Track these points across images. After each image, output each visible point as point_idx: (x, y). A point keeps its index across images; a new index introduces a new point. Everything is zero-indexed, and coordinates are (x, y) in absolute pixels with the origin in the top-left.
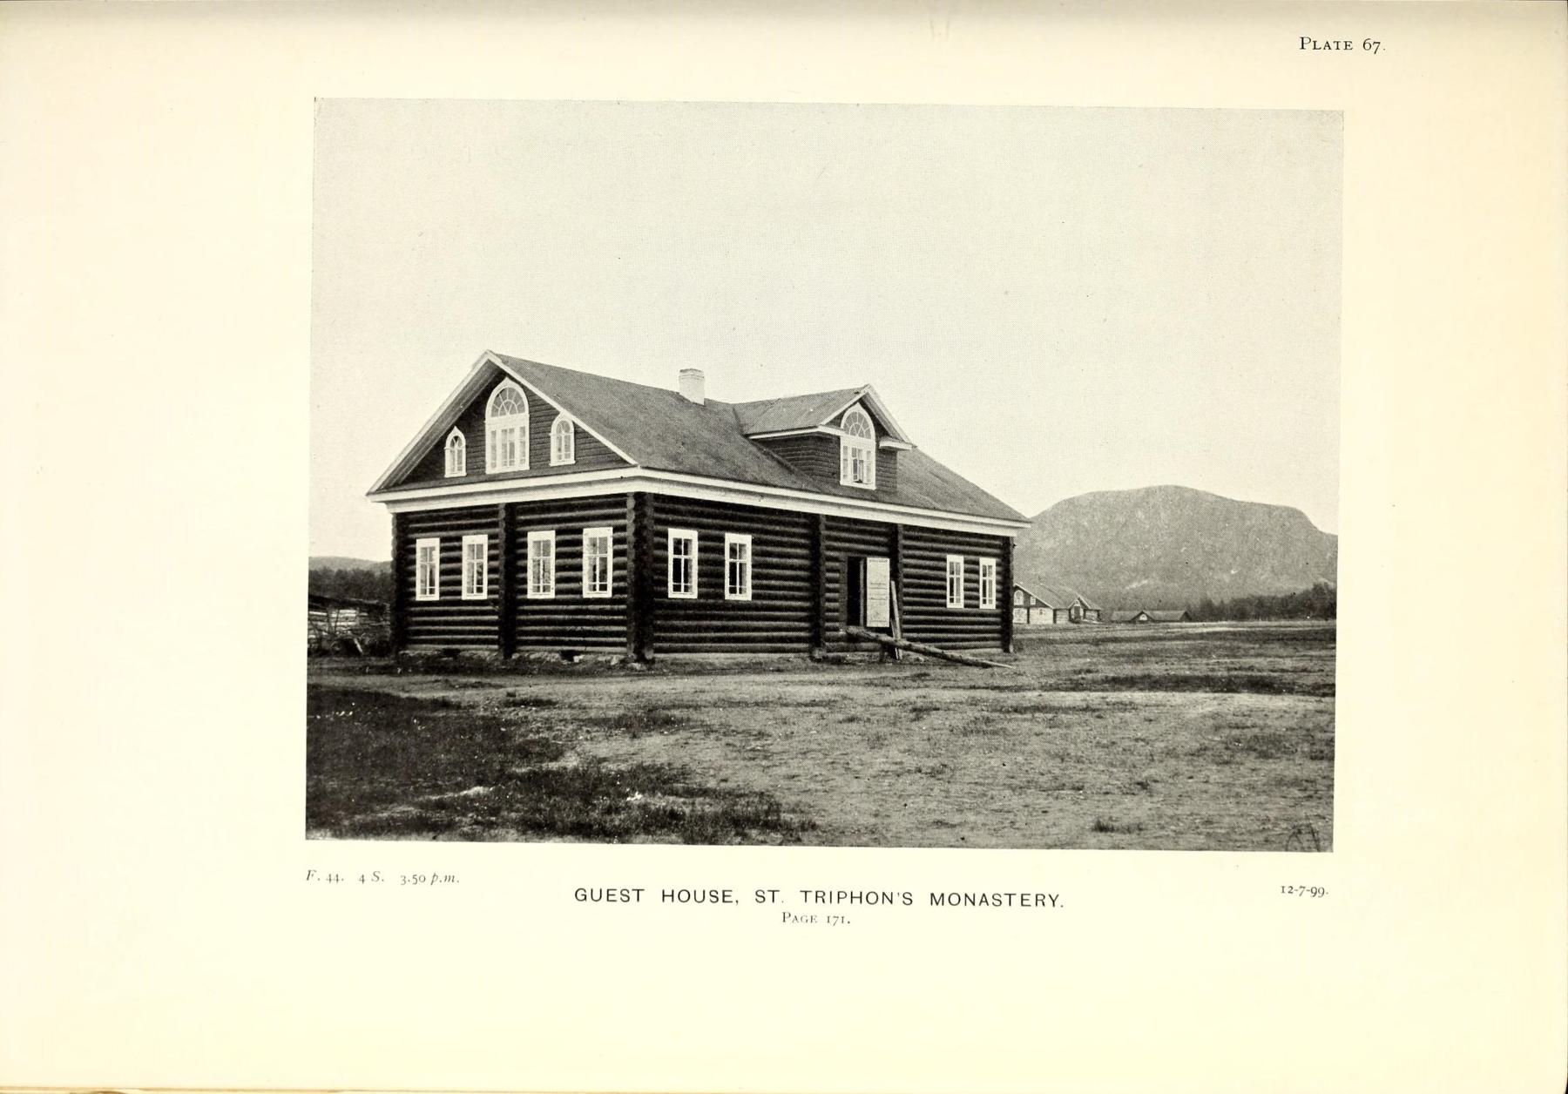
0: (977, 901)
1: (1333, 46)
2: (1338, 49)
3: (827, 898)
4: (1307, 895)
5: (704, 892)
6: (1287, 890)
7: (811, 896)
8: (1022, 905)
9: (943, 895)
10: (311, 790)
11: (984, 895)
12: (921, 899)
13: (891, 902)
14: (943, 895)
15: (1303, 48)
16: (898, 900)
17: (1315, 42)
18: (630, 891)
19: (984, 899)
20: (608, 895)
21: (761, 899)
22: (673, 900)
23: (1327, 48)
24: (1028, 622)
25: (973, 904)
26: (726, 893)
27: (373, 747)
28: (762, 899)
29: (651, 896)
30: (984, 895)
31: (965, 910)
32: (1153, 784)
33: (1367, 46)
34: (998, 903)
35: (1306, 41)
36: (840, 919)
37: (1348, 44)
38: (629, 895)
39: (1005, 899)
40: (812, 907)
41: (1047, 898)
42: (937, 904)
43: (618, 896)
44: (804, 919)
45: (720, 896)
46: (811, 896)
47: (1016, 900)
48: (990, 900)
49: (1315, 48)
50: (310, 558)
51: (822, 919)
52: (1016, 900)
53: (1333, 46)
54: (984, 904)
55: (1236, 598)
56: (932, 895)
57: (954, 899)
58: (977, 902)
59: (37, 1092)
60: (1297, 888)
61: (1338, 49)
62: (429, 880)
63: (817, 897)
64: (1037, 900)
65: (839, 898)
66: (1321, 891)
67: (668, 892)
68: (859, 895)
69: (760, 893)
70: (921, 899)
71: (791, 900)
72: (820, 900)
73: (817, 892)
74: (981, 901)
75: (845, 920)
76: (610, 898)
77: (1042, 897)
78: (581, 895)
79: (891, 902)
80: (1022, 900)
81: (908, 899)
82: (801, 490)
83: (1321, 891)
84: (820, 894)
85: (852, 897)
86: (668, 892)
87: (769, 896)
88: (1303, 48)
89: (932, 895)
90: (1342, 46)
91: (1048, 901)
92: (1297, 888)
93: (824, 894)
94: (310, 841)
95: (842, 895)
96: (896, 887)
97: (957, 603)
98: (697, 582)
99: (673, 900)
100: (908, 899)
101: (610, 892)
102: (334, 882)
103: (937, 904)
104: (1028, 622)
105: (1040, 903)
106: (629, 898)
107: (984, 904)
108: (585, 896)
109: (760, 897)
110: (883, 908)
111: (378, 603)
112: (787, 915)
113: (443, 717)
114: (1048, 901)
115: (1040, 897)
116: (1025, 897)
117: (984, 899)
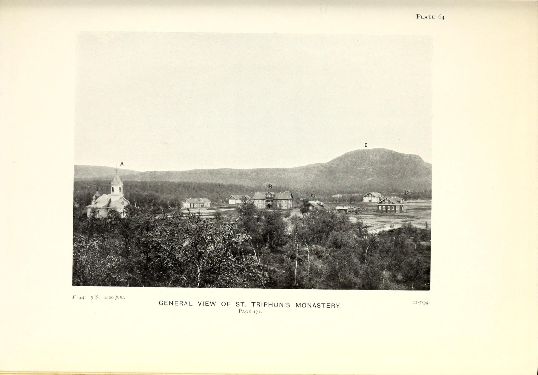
0: (312, 306)
2: (430, 18)
3: (261, 305)
5: (162, 303)
6: (415, 302)
7: (255, 304)
8: (327, 307)
9: (300, 304)
11: (314, 304)
12: (293, 305)
13: (283, 306)
14: (300, 304)
15: (418, 18)
16: (285, 306)
19: (314, 305)
20: (206, 304)
21: (238, 305)
25: (311, 307)
27: (239, 257)
29: (218, 304)
30: (314, 304)
31: (308, 309)
34: (319, 307)
35: (419, 16)
36: (258, 312)
37: (433, 16)
38: (320, 305)
39: (322, 305)
40: (256, 308)
41: (336, 305)
42: (298, 307)
43: (209, 304)
44: (247, 312)
46: (255, 304)
47: (325, 305)
48: (316, 306)
50: (76, 167)
52: (325, 305)
54: (314, 307)
55: (416, 227)
56: (297, 304)
57: (276, 305)
58: (312, 306)
59: (179, 374)
60: (419, 302)
61: (430, 18)
62: (115, 298)
63: (257, 304)
64: (180, 303)
65: (265, 305)
66: (427, 303)
67: (270, 303)
68: (228, 305)
69: (238, 303)
71: (248, 306)
72: (258, 305)
73: (180, 302)
74: (313, 306)
75: (260, 312)
76: (207, 305)
77: (182, 302)
79: (283, 306)
80: (327, 305)
81: (288, 305)
83: (427, 303)
84: (258, 303)
85: (269, 305)
86: (270, 303)
88: (418, 18)
89: (297, 304)
90: (431, 17)
91: (336, 306)
92: (419, 302)
93: (335, 305)
94: (74, 286)
95: (266, 304)
96: (285, 302)
98: (205, 199)
100: (288, 305)
101: (228, 303)
102: (82, 299)
103: (298, 307)
105: (333, 307)
106: (320, 306)
107: (314, 307)
108: (163, 303)
109: (238, 304)
111: (336, 206)
112: (241, 310)
113: (367, 251)
114: (336, 306)
115: (333, 305)
117: (314, 305)
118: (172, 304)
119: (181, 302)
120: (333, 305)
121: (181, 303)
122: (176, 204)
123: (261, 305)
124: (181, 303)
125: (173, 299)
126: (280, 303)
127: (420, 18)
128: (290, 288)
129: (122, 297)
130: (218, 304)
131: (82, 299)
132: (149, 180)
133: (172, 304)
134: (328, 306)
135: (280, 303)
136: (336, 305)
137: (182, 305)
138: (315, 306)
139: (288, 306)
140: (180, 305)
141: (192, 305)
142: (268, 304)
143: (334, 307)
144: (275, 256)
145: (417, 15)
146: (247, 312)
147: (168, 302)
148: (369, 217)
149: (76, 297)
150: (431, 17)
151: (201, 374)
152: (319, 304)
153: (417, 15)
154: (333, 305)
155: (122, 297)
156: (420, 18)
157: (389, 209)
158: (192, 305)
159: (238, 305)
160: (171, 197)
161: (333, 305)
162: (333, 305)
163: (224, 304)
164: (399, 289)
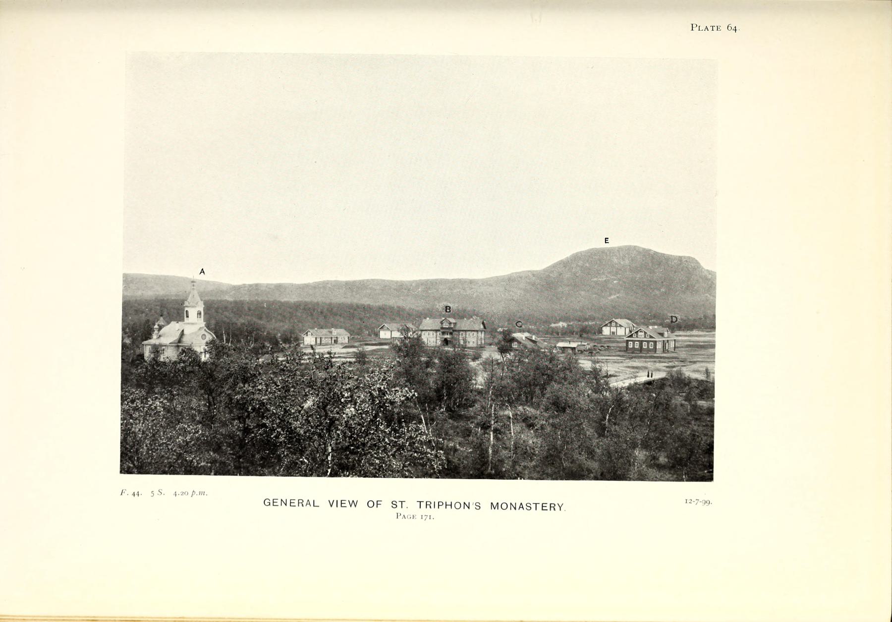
0: (518, 507)
3: (432, 505)
4: (700, 504)
5: (268, 503)
7: (423, 505)
8: (542, 509)
9: (498, 503)
10: (535, 475)
11: (521, 504)
12: (485, 506)
13: (469, 508)
14: (498, 503)
15: (692, 30)
16: (472, 507)
17: (699, 26)
19: (521, 505)
20: (341, 503)
21: (395, 506)
23: (706, 30)
25: (515, 508)
28: (479, 508)
29: (362, 505)
30: (521, 504)
33: (730, 28)
34: (529, 508)
35: (694, 26)
36: (429, 517)
37: (719, 27)
39: (533, 506)
40: (424, 511)
41: (557, 505)
42: (495, 509)
43: (347, 504)
44: (409, 517)
46: (423, 505)
47: (539, 506)
48: (525, 507)
52: (539, 506)
56: (492, 503)
57: (504, 506)
61: (713, 30)
62: (190, 494)
63: (427, 505)
66: (708, 502)
67: (449, 503)
71: (412, 507)
72: (428, 506)
74: (520, 507)
76: (343, 505)
77: (430, 503)
79: (469, 508)
80: (542, 506)
82: (608, 356)
83: (708, 502)
84: (428, 503)
85: (446, 505)
86: (449, 503)
88: (692, 30)
89: (492, 503)
90: (715, 28)
91: (557, 507)
93: (431, 503)
94: (122, 475)
95: (441, 504)
100: (478, 506)
101: (378, 503)
102: (136, 496)
103: (495, 509)
104: (316, 338)
105: (552, 509)
106: (480, 507)
108: (270, 503)
112: (399, 515)
115: (552, 505)
117: (308, 503)
118: (286, 505)
119: (301, 501)
121: (300, 502)
122: (292, 339)
123: (432, 505)
124: (300, 502)
125: (287, 497)
126: (464, 503)
127: (696, 29)
129: (202, 493)
130: (362, 505)
131: (136, 496)
132: (247, 299)
133: (286, 505)
134: (544, 508)
136: (557, 505)
137: (430, 507)
138: (309, 504)
139: (478, 508)
140: (550, 510)
141: (536, 509)
143: (554, 509)
145: (692, 25)
146: (409, 517)
147: (296, 502)
148: (612, 361)
150: (715, 28)
153: (692, 25)
154: (552, 506)
155: (202, 493)
156: (696, 29)
158: (402, 507)
160: (283, 326)
161: (552, 505)
162: (552, 506)
163: (371, 504)
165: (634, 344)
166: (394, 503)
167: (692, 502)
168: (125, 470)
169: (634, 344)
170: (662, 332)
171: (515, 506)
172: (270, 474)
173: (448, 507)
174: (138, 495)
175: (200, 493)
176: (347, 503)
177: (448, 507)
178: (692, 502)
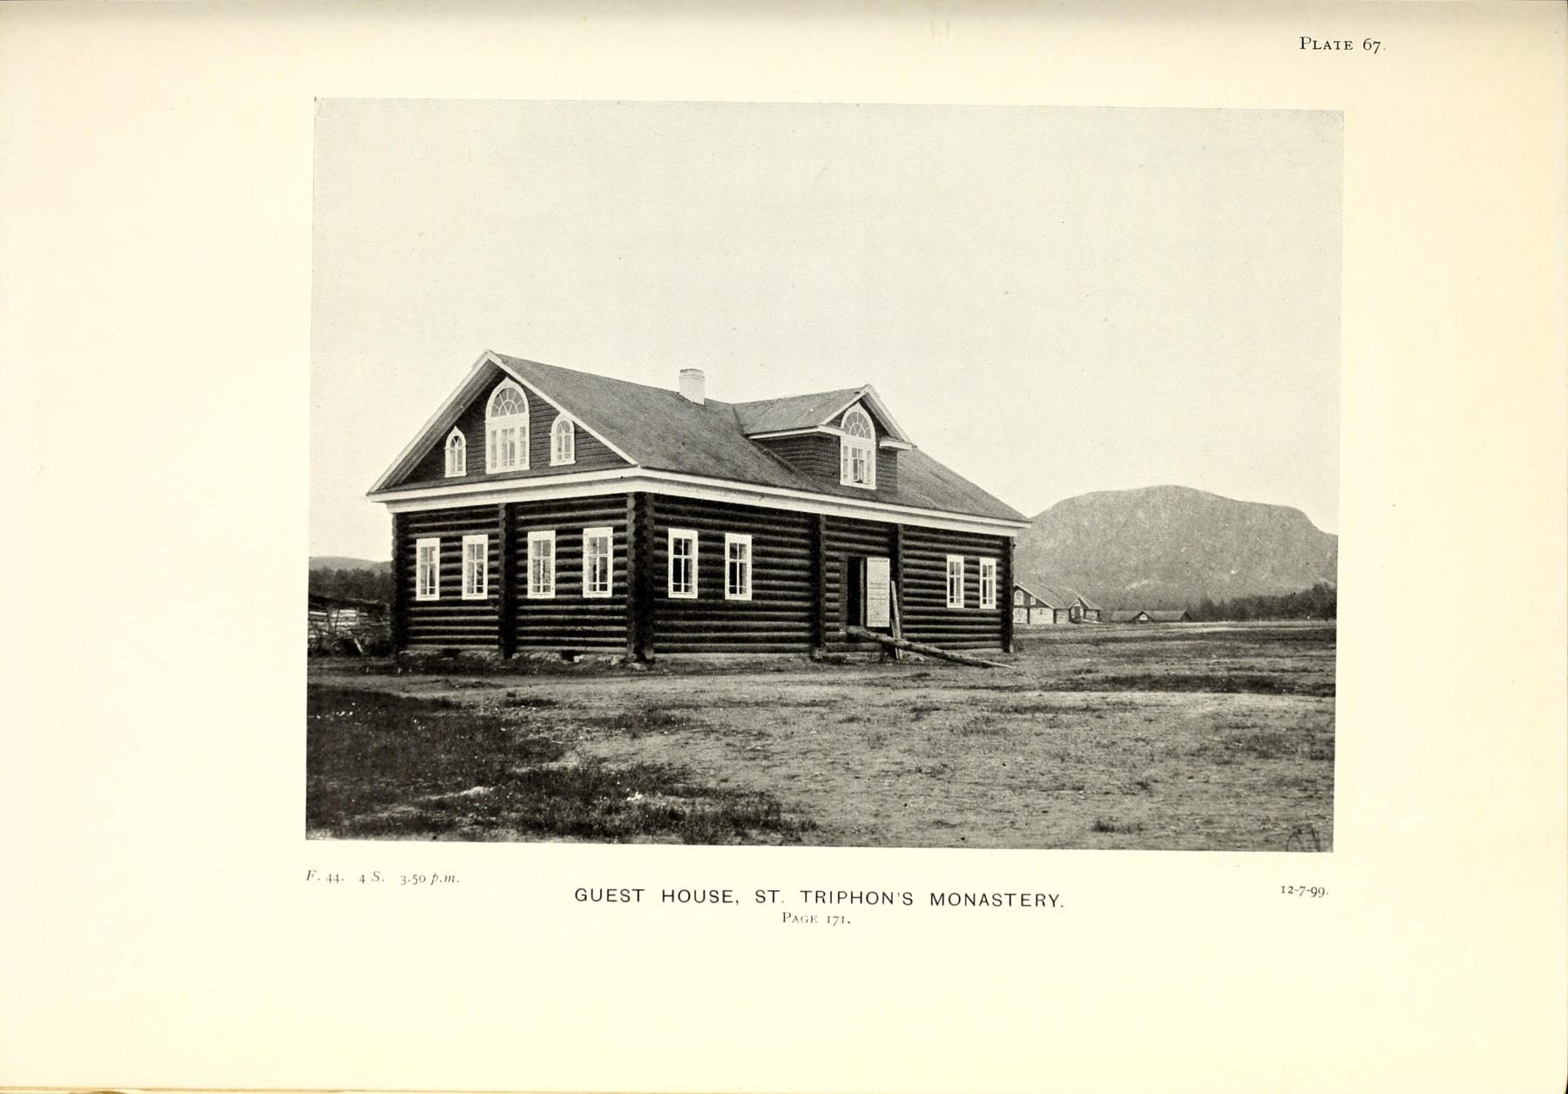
0: (978, 901)
1: (1334, 46)
2: (1338, 48)
3: (827, 898)
6: (1287, 890)
7: (811, 896)
9: (943, 895)
11: (984, 895)
12: (921, 899)
13: (891, 902)
14: (943, 895)
16: (898, 900)
17: (1315, 42)
18: (630, 891)
19: (984, 899)
20: (608, 895)
21: (762, 899)
22: (673, 901)
23: (1327, 48)
24: (1029, 622)
25: (974, 904)
26: (726, 893)
28: (909, 902)
29: (651, 896)
30: (984, 895)
31: (965, 910)
32: (1154, 784)
33: (1367, 46)
34: (998, 903)
35: (1306, 40)
38: (993, 901)
39: (1005, 899)
40: (812, 907)
41: (1048, 898)
42: (937, 904)
43: (618, 896)
44: (804, 919)
45: (720, 896)
46: (811, 896)
47: (1016, 900)
48: (990, 900)
49: (1315, 48)
51: (822, 920)
52: (1016, 900)
53: (1334, 46)
54: (984, 904)
56: (933, 895)
57: (955, 899)
58: (977, 902)
59: (37, 1092)
61: (1338, 48)
62: (429, 880)
63: (817, 897)
65: (839, 898)
66: (1321, 891)
67: (856, 894)
68: (671, 894)
70: (921, 899)
71: (791, 900)
72: (820, 900)
74: (982, 901)
76: (610, 898)
77: (822, 894)
78: (581, 895)
79: (891, 902)
80: (1022, 900)
81: (908, 899)
83: (1321, 891)
84: (820, 894)
86: (856, 894)
87: (769, 896)
88: (1303, 48)
89: (933, 895)
90: (1342, 45)
94: (310, 841)
95: (842, 895)
96: (895, 887)
97: (957, 603)
99: (673, 901)
100: (908, 899)
101: (610, 893)
102: (334, 882)
103: (937, 904)
104: (1029, 622)
105: (1040, 903)
107: (984, 904)
108: (586, 896)
110: (883, 908)
112: (787, 915)
114: (1048, 901)
115: (1040, 897)
116: (1025, 897)
117: (984, 899)
120: (1040, 897)
126: (884, 894)
128: (310, 820)
135: (884, 894)
138: (986, 901)
139: (908, 902)
142: (849, 896)
143: (1044, 904)
144: (541, 735)
149: (316, 876)
151: (255, 1091)
152: (996, 897)
157: (540, 585)
159: (761, 899)
164: (1031, 842)
165: (569, 551)
166: (625, 893)
167: (1293, 891)
168: (1336, 537)
169: (569, 551)
170: (1302, 586)
171: (968, 899)
172: (749, 844)
173: (856, 901)
174: (363, 881)
175: (417, 879)
176: (618, 893)
177: (856, 901)
178: (1293, 891)
